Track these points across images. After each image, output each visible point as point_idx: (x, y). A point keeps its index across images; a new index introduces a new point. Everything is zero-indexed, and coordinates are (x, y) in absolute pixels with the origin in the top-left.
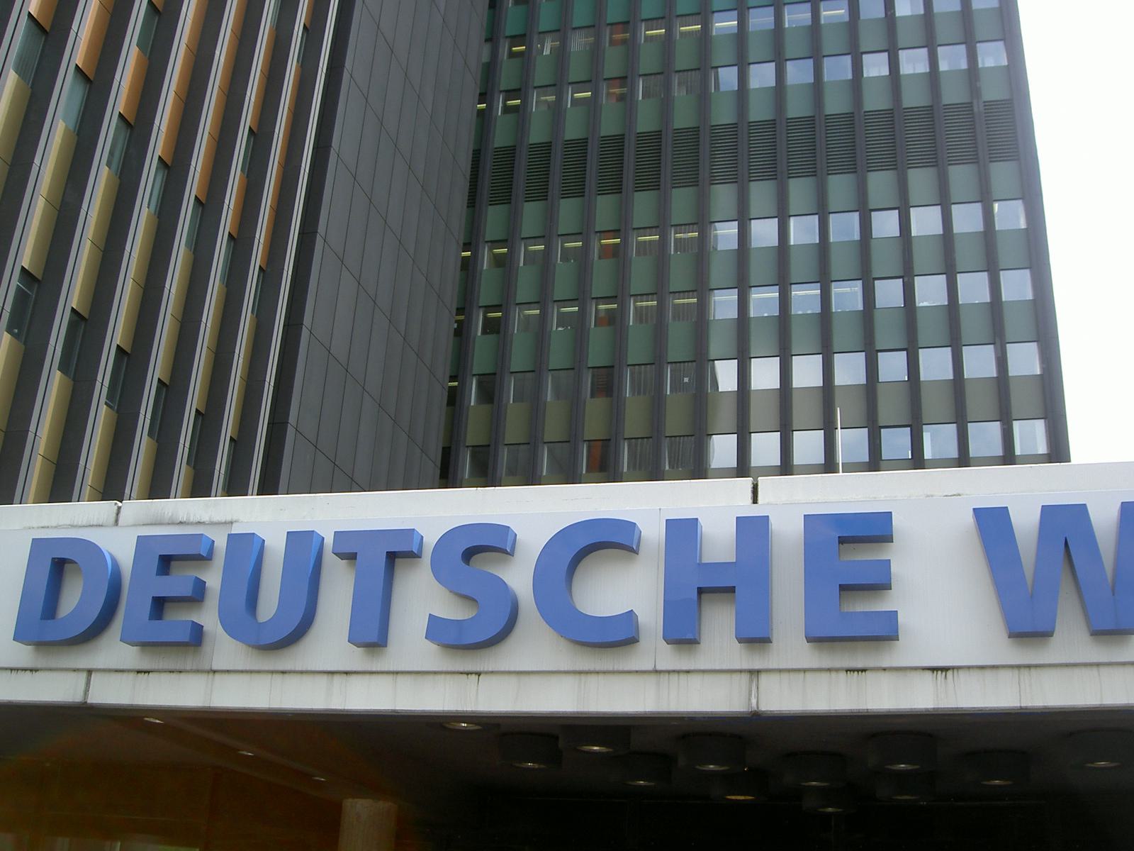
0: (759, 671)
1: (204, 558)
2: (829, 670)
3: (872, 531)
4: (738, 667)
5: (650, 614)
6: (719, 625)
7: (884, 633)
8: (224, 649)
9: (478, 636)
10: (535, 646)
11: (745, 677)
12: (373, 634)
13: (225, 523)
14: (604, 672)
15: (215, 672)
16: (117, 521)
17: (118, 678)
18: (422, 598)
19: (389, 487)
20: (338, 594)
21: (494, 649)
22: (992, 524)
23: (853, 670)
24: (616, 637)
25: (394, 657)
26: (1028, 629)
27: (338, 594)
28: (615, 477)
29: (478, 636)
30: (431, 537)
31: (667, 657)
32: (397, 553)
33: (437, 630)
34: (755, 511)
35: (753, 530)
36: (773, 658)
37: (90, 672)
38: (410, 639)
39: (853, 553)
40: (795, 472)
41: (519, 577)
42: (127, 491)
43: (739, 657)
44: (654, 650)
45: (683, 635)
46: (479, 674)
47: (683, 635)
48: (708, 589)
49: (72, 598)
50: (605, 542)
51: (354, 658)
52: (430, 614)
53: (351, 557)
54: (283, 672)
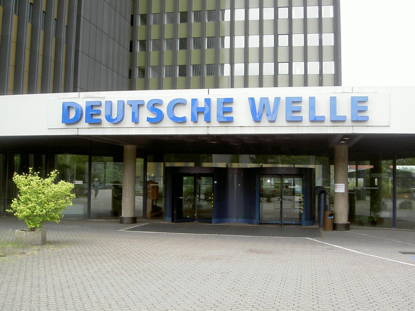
0: (209, 127)
1: (100, 105)
2: (333, 126)
3: (229, 101)
4: (205, 126)
5: (189, 117)
6: (201, 118)
7: (230, 120)
8: (105, 123)
9: (157, 120)
10: (83, 124)
11: (352, 127)
12: (135, 120)
13: (103, 97)
14: (357, 126)
15: (104, 128)
16: (79, 97)
17: (84, 130)
18: (145, 114)
19: (112, 90)
20: (128, 112)
21: (120, 123)
22: (252, 100)
23: (226, 127)
24: (183, 121)
25: (140, 124)
26: (257, 120)
27: (128, 112)
28: (68, 91)
29: (157, 120)
30: (146, 102)
31: (192, 124)
32: (140, 105)
33: (149, 120)
34: (208, 97)
35: (277, 100)
36: (211, 125)
37: (78, 128)
38: (143, 121)
39: (226, 106)
40: (249, 87)
41: (164, 109)
42: (60, 90)
43: (205, 124)
44: (189, 122)
45: (195, 120)
46: (157, 127)
47: (195, 120)
48: (200, 112)
49: (72, 114)
50: (179, 103)
51: (133, 124)
52: (148, 117)
53: (131, 105)
54: (119, 128)
